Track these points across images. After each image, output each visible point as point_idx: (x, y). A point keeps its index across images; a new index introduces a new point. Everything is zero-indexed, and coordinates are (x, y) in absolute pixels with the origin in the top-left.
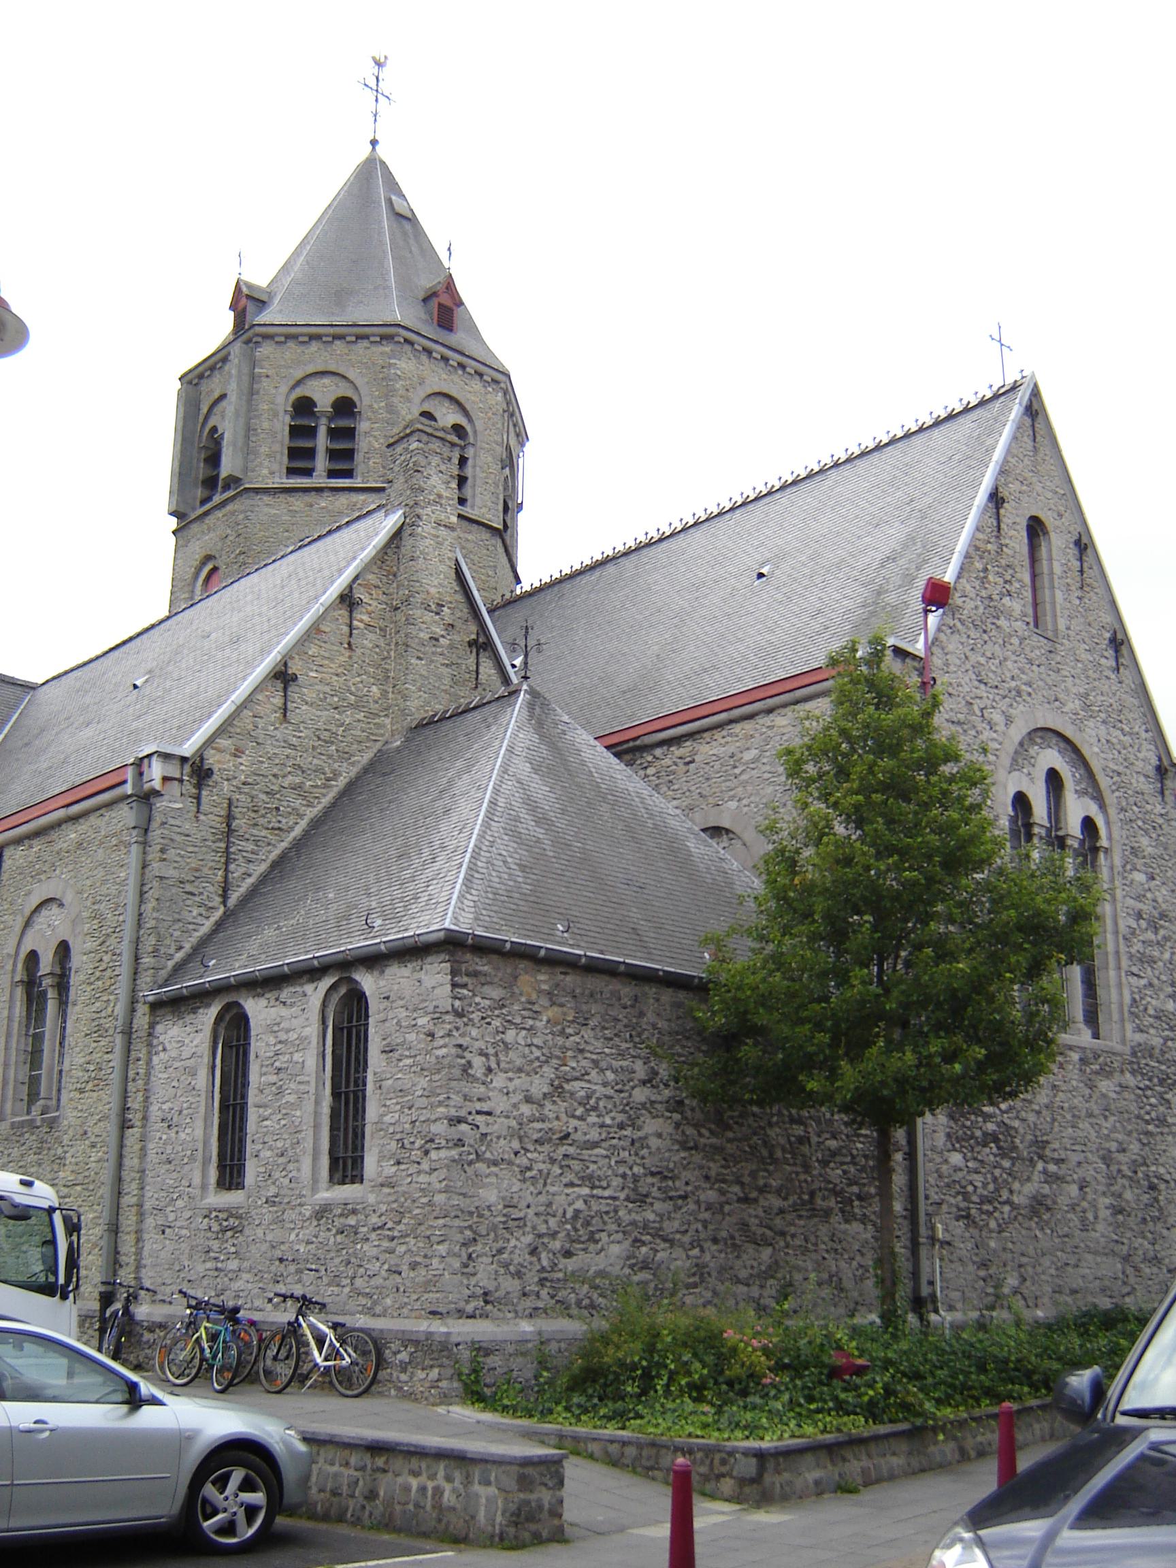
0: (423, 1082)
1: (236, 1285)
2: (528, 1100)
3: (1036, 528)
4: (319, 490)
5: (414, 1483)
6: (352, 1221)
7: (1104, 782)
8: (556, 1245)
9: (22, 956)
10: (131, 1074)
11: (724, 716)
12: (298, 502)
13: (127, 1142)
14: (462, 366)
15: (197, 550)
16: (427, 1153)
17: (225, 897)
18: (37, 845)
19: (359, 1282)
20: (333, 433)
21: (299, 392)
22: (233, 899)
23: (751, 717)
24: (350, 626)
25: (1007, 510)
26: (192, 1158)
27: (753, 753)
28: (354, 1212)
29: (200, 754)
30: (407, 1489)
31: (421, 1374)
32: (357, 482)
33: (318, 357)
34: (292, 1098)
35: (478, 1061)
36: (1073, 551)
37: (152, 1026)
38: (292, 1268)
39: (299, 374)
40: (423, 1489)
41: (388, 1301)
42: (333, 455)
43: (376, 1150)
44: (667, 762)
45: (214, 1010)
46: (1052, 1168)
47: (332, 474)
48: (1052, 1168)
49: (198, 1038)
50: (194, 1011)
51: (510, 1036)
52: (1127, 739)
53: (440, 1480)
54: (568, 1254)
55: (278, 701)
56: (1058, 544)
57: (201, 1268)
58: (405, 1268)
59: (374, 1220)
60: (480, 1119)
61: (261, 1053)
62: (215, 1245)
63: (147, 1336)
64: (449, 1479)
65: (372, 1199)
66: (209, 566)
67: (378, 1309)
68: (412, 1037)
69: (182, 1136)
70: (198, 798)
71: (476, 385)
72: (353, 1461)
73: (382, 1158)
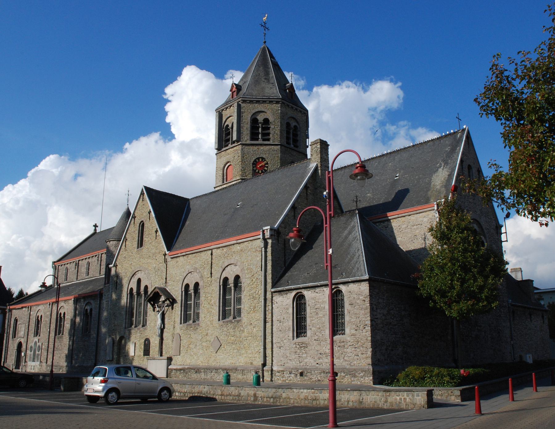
0: (363, 312)
1: (306, 360)
2: (384, 315)
3: (470, 167)
4: (261, 145)
5: (398, 398)
6: (343, 344)
7: (486, 231)
8: (390, 348)
9: (222, 278)
10: (267, 309)
11: (397, 216)
12: (255, 148)
13: (267, 326)
14: (296, 109)
15: (224, 160)
16: (365, 328)
17: (285, 264)
18: (225, 249)
19: (346, 358)
20: (263, 129)
21: (254, 117)
22: (286, 265)
23: (404, 216)
24: (307, 194)
25: (464, 163)
26: (289, 330)
27: (405, 226)
28: (343, 342)
29: (278, 229)
30: (396, 399)
31: (367, 378)
32: (271, 142)
33: (259, 107)
34: (321, 316)
35: (375, 307)
36: (477, 173)
37: (272, 297)
38: (324, 356)
39: (254, 112)
40: (401, 399)
41: (355, 362)
42: (263, 135)
43: (349, 327)
44: (380, 227)
45: (294, 293)
46: (479, 328)
47: (264, 140)
48: (479, 328)
49: (288, 301)
50: (286, 294)
51: (380, 300)
52: (489, 220)
53: (405, 396)
54: (392, 350)
55: (293, 214)
56: (474, 170)
57: (294, 357)
58: (360, 355)
59: (349, 344)
60: (376, 320)
61: (310, 305)
62: (299, 351)
63: (277, 374)
64: (408, 396)
65: (348, 339)
66: (229, 164)
67: (352, 364)
68: (358, 301)
69: (285, 325)
70: (278, 240)
71: (300, 114)
72: (380, 394)
73: (351, 329)
